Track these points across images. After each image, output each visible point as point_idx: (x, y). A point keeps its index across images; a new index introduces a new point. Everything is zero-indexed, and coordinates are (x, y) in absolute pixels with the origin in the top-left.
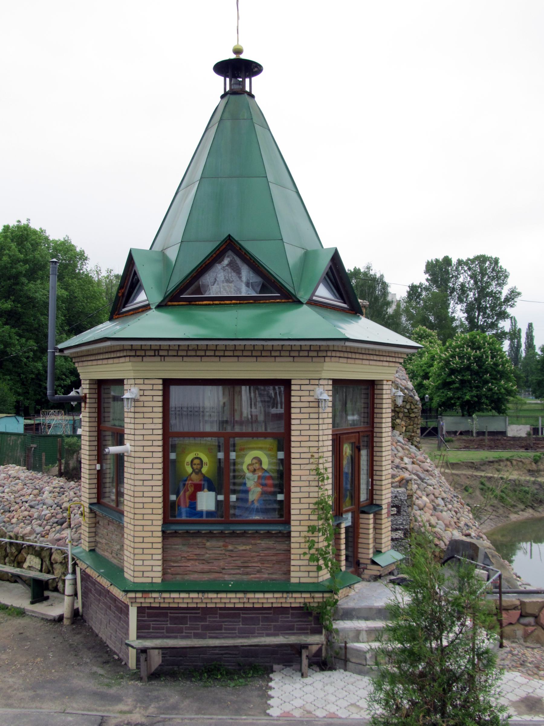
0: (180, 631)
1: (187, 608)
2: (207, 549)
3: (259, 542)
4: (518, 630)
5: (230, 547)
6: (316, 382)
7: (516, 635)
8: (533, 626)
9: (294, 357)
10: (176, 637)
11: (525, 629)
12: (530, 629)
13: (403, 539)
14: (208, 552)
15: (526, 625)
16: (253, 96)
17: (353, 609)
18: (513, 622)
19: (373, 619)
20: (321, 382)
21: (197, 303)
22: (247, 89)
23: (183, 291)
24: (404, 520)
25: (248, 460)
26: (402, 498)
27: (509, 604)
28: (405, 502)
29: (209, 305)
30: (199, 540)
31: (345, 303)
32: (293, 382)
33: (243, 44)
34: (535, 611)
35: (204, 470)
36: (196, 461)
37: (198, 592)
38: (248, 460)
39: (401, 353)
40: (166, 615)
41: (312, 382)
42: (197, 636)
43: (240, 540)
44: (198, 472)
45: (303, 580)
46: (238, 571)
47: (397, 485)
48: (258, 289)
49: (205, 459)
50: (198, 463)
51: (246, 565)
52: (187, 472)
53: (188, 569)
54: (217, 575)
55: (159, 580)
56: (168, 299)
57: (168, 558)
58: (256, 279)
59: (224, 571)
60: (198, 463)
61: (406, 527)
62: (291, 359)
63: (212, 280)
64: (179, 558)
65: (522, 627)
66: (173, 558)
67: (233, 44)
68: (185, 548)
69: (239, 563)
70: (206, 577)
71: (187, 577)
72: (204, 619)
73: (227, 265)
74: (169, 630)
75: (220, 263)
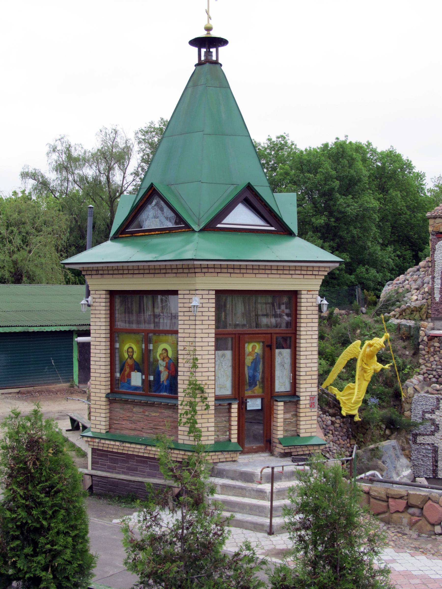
0: (114, 468)
1: (117, 453)
2: (134, 413)
3: (163, 411)
4: (404, 518)
5: (147, 413)
6: (194, 292)
7: (402, 522)
8: (418, 516)
9: (243, 273)
10: (112, 472)
11: (410, 518)
12: (414, 519)
14: (134, 415)
15: (413, 515)
16: (221, 65)
17: (224, 470)
18: (401, 510)
19: (237, 480)
20: (197, 292)
21: (138, 234)
22: (214, 58)
23: (128, 226)
25: (126, 347)
27: (396, 493)
29: (143, 236)
30: (129, 406)
31: (272, 226)
32: (179, 292)
33: (212, 23)
34: (418, 503)
35: (135, 356)
36: (130, 350)
37: (120, 441)
38: (126, 347)
39: (325, 267)
40: (106, 456)
41: (192, 292)
42: (124, 473)
43: (153, 409)
44: (131, 357)
45: (186, 442)
46: (151, 431)
48: (173, 221)
49: (135, 348)
50: (131, 351)
51: (156, 427)
52: (125, 357)
53: (124, 426)
54: (139, 432)
55: (104, 431)
56: (120, 232)
57: (113, 417)
58: (171, 214)
59: (143, 430)
60: (131, 351)
62: (241, 275)
63: (146, 217)
64: (118, 418)
65: (409, 516)
66: (115, 418)
67: (204, 23)
68: (122, 411)
69: (152, 425)
70: (133, 433)
71: (122, 432)
72: (127, 462)
73: (155, 205)
74: (109, 467)
75: (151, 204)
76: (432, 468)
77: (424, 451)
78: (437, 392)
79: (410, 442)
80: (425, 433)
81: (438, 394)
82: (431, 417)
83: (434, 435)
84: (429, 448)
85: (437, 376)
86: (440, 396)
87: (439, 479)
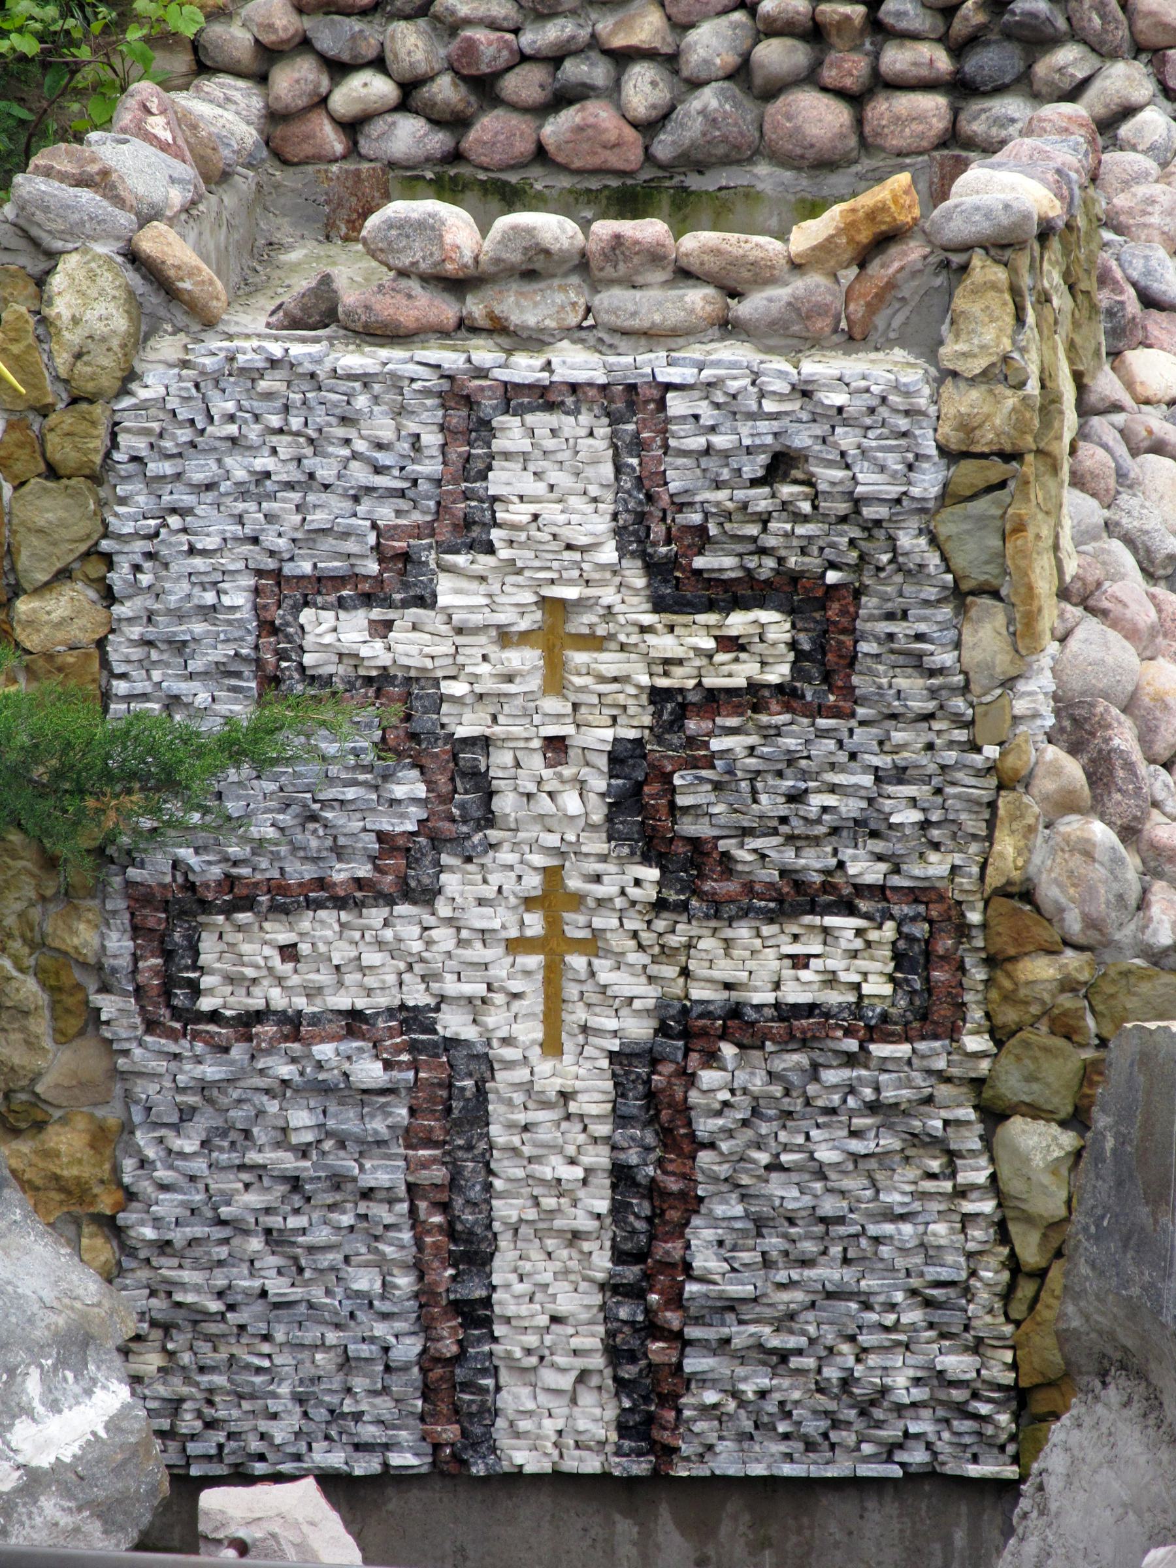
13: (880, 1030)
24: (901, 775)
26: (869, 481)
28: (909, 540)
47: (800, 311)
61: (937, 866)
76: (408, 1349)
77: (301, 1118)
78: (446, 310)
79: (109, 1006)
80: (300, 872)
81: (466, 327)
82: (375, 653)
83: (427, 896)
84: (370, 1072)
85: (445, 90)
86: (485, 354)
87: (517, 1477)
